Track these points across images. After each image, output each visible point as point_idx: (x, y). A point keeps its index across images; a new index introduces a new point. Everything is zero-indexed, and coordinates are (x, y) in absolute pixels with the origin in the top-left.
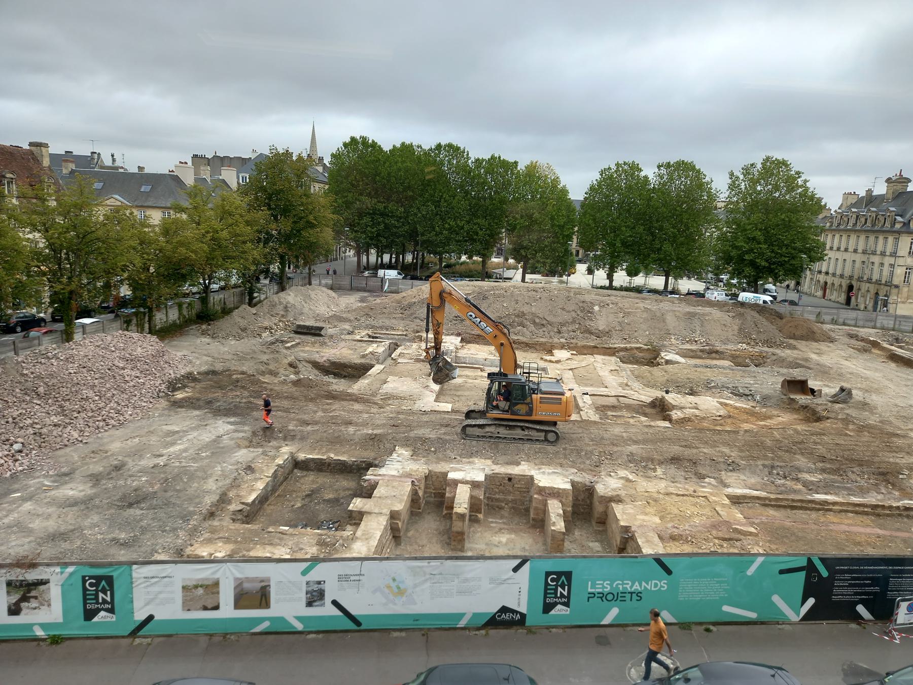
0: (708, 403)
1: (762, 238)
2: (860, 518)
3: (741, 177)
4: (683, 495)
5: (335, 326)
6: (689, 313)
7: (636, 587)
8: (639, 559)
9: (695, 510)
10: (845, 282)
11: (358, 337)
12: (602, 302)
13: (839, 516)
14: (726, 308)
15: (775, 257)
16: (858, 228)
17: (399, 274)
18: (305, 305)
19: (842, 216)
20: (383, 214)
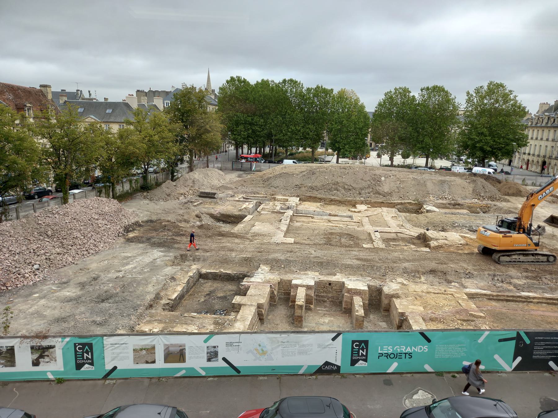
3: (474, 95)
4: (438, 293)
5: (223, 192)
6: (441, 180)
7: (409, 350)
8: (410, 333)
9: (445, 302)
10: (541, 160)
11: (237, 199)
12: (386, 174)
13: (537, 305)
15: (496, 145)
18: (205, 180)
20: (251, 124)
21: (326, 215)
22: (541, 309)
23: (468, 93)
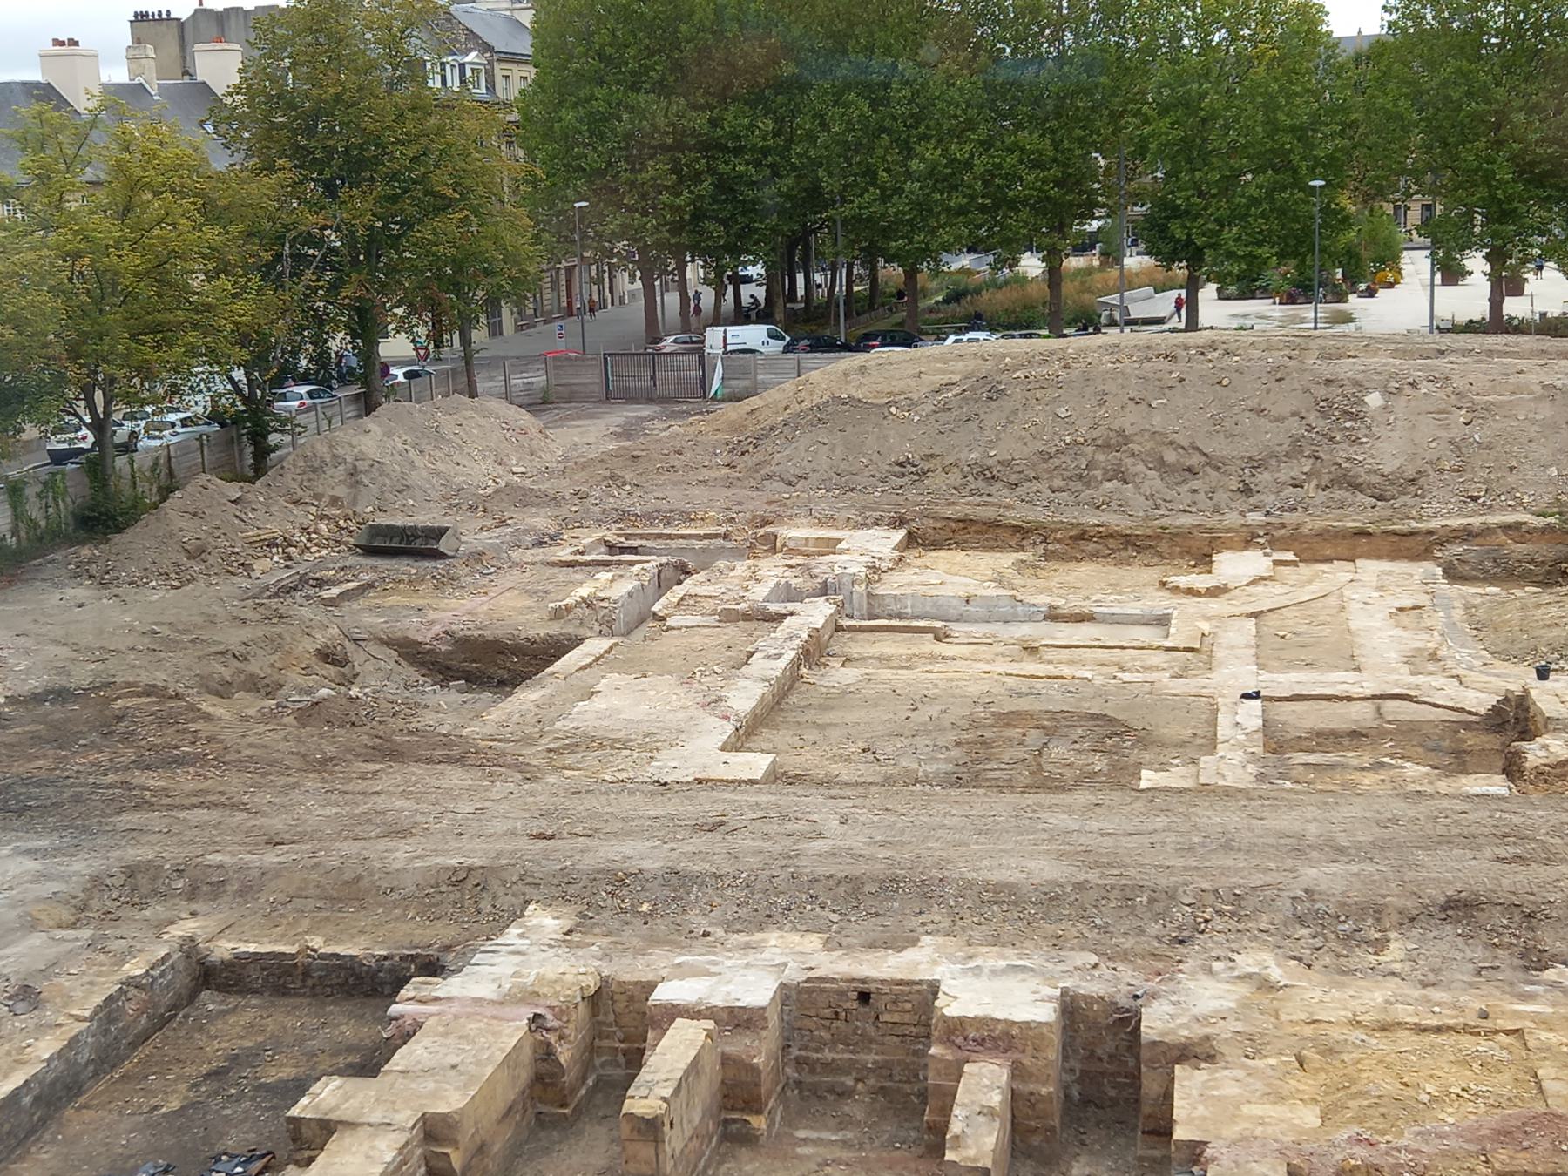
4: (1439, 1030)
5: (503, 523)
9: (1457, 1079)
11: (564, 554)
17: (773, 335)
18: (420, 462)
20: (711, 147)
21: (1030, 619)
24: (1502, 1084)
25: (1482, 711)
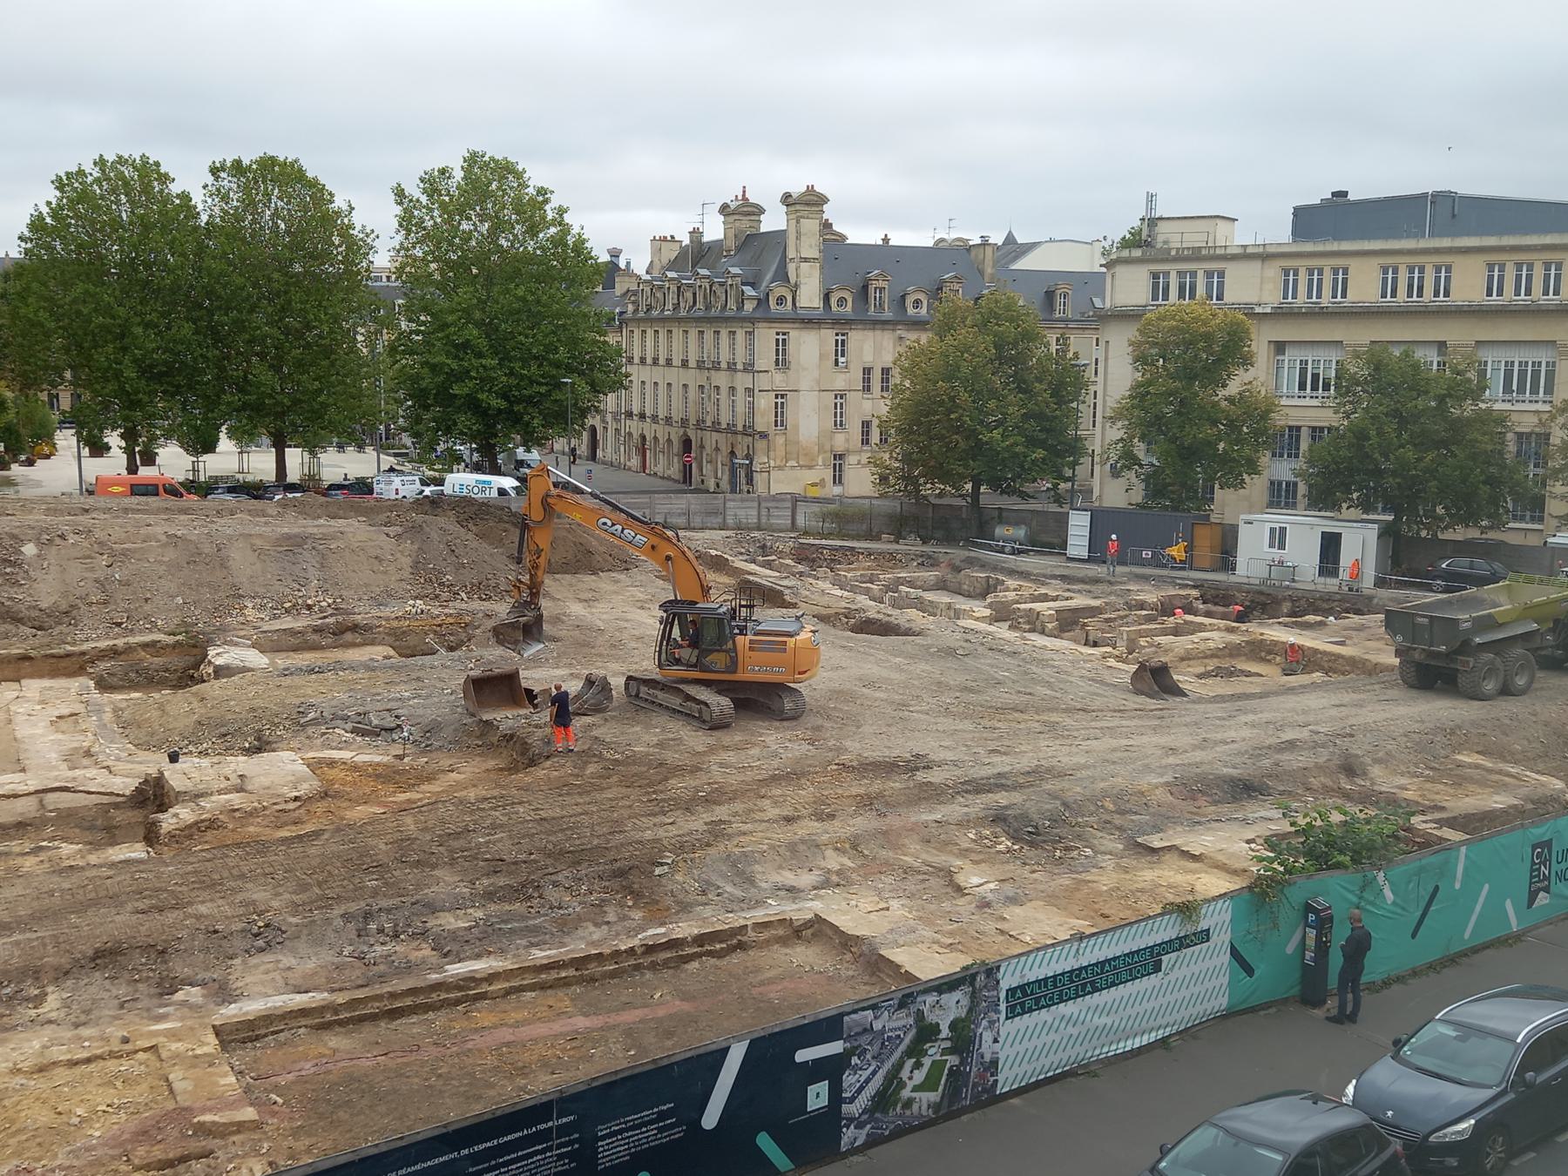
0: (283, 770)
1: (483, 343)
2: (551, 997)
3: (424, 199)
4: (88, 1061)
6: (288, 537)
9: (102, 1098)
10: (676, 434)
12: (46, 530)
13: (503, 1004)
14: (383, 517)
16: (683, 313)
19: (655, 286)
22: (516, 1016)
23: (400, 194)
24: (140, 1094)
25: (128, 793)
